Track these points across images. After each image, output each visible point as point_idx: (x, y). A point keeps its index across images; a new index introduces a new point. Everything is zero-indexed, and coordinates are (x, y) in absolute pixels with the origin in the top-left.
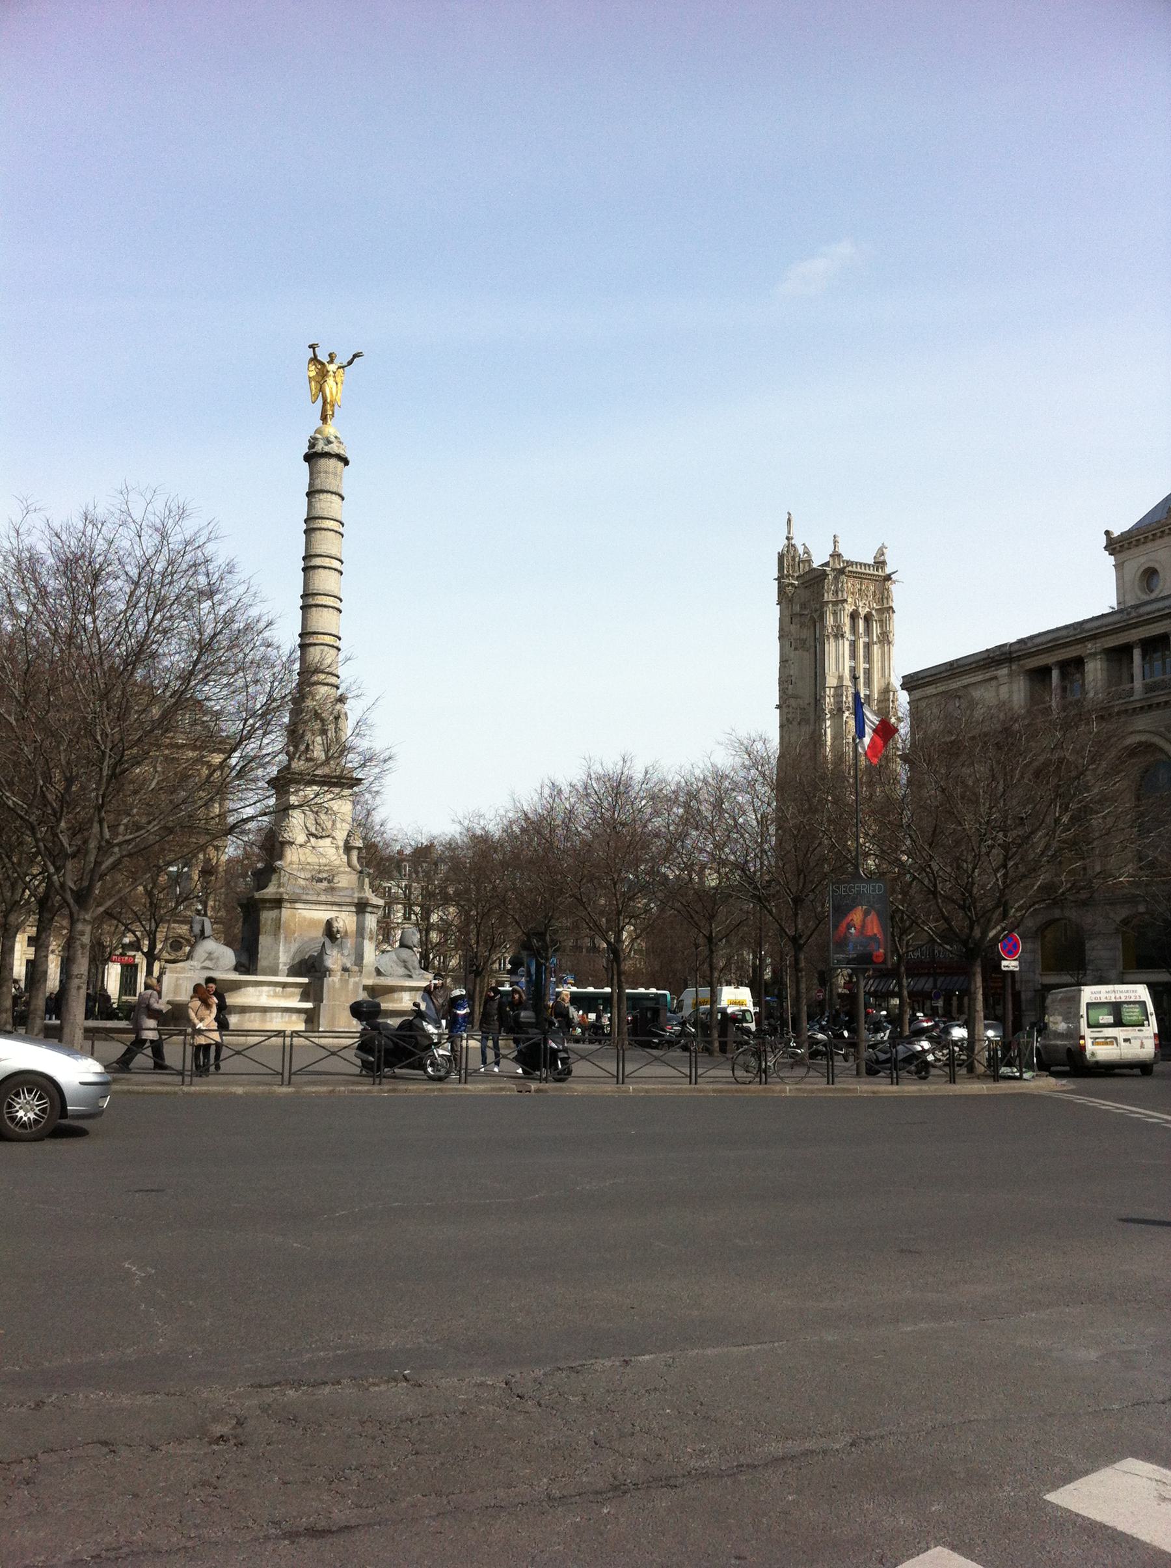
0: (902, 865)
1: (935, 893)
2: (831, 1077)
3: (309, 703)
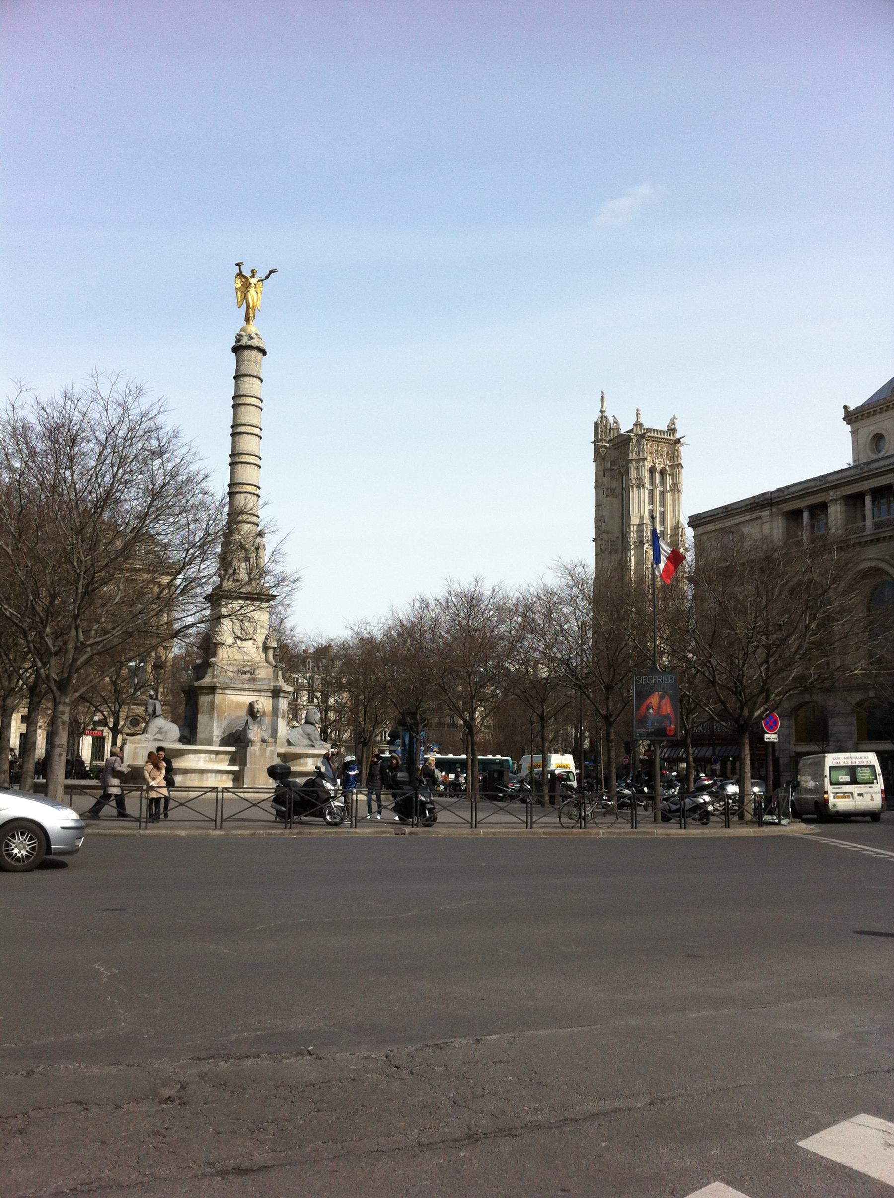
0: (689, 661)
1: (713, 682)
2: (634, 823)
3: (236, 537)
